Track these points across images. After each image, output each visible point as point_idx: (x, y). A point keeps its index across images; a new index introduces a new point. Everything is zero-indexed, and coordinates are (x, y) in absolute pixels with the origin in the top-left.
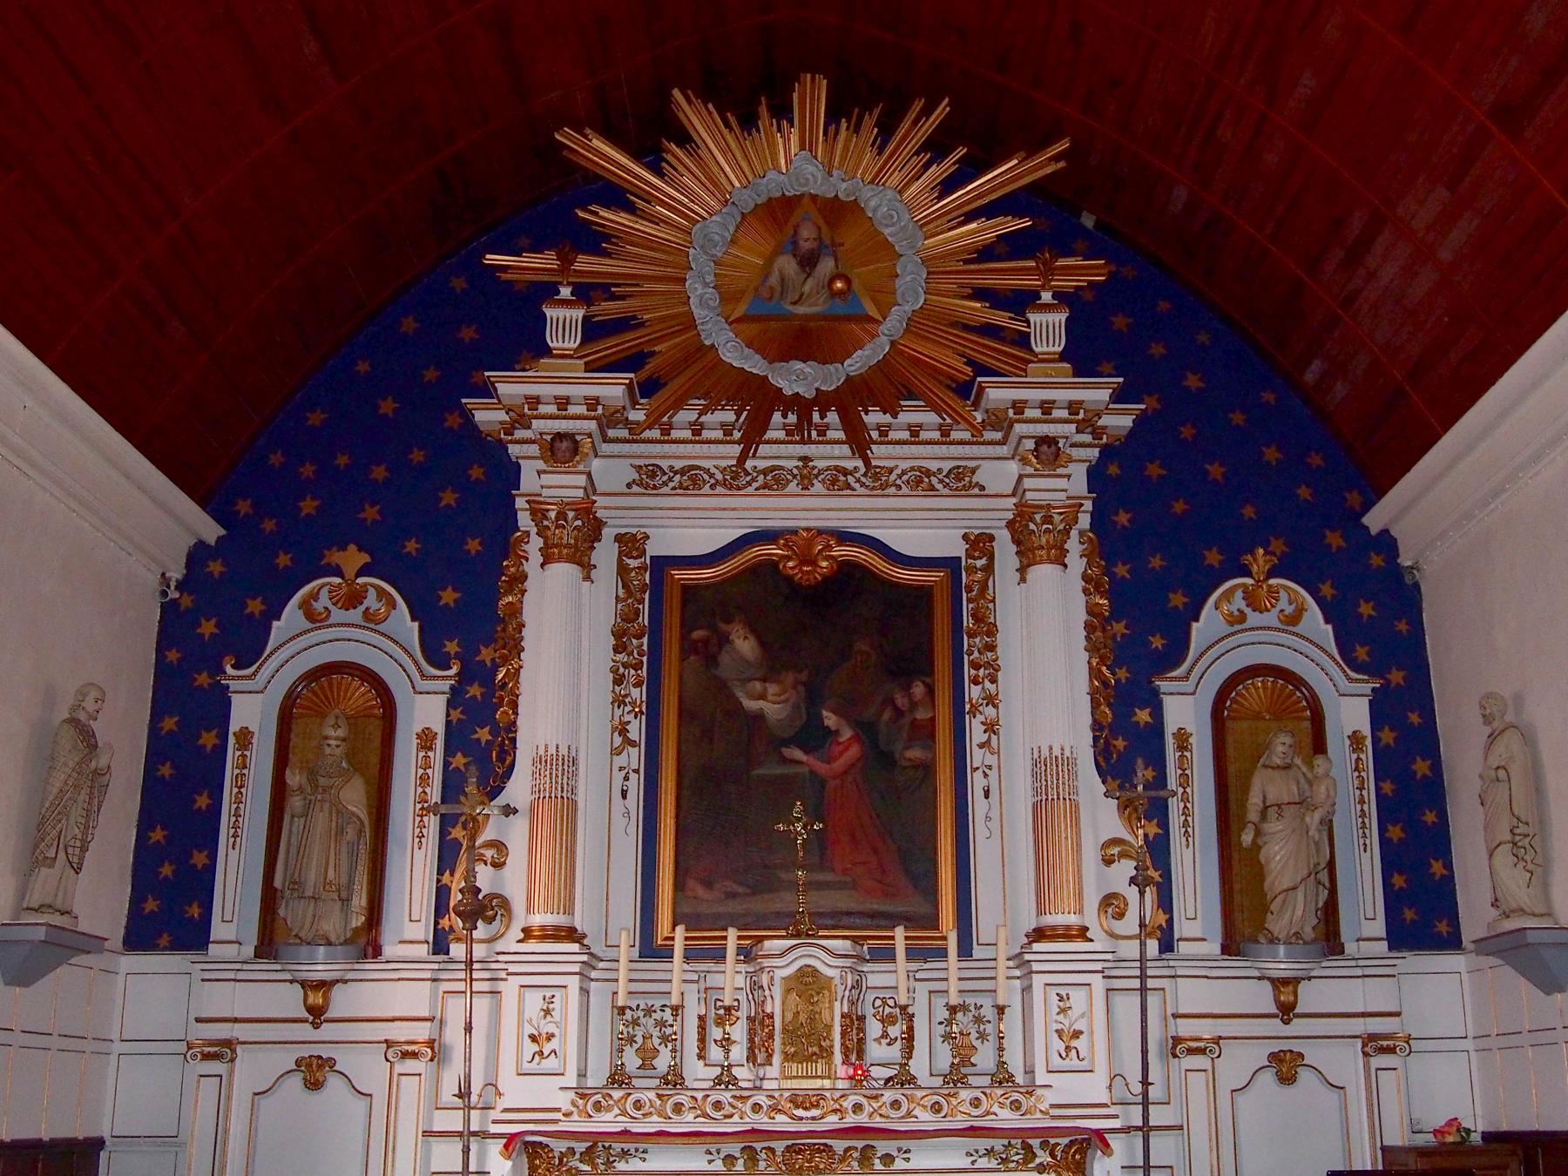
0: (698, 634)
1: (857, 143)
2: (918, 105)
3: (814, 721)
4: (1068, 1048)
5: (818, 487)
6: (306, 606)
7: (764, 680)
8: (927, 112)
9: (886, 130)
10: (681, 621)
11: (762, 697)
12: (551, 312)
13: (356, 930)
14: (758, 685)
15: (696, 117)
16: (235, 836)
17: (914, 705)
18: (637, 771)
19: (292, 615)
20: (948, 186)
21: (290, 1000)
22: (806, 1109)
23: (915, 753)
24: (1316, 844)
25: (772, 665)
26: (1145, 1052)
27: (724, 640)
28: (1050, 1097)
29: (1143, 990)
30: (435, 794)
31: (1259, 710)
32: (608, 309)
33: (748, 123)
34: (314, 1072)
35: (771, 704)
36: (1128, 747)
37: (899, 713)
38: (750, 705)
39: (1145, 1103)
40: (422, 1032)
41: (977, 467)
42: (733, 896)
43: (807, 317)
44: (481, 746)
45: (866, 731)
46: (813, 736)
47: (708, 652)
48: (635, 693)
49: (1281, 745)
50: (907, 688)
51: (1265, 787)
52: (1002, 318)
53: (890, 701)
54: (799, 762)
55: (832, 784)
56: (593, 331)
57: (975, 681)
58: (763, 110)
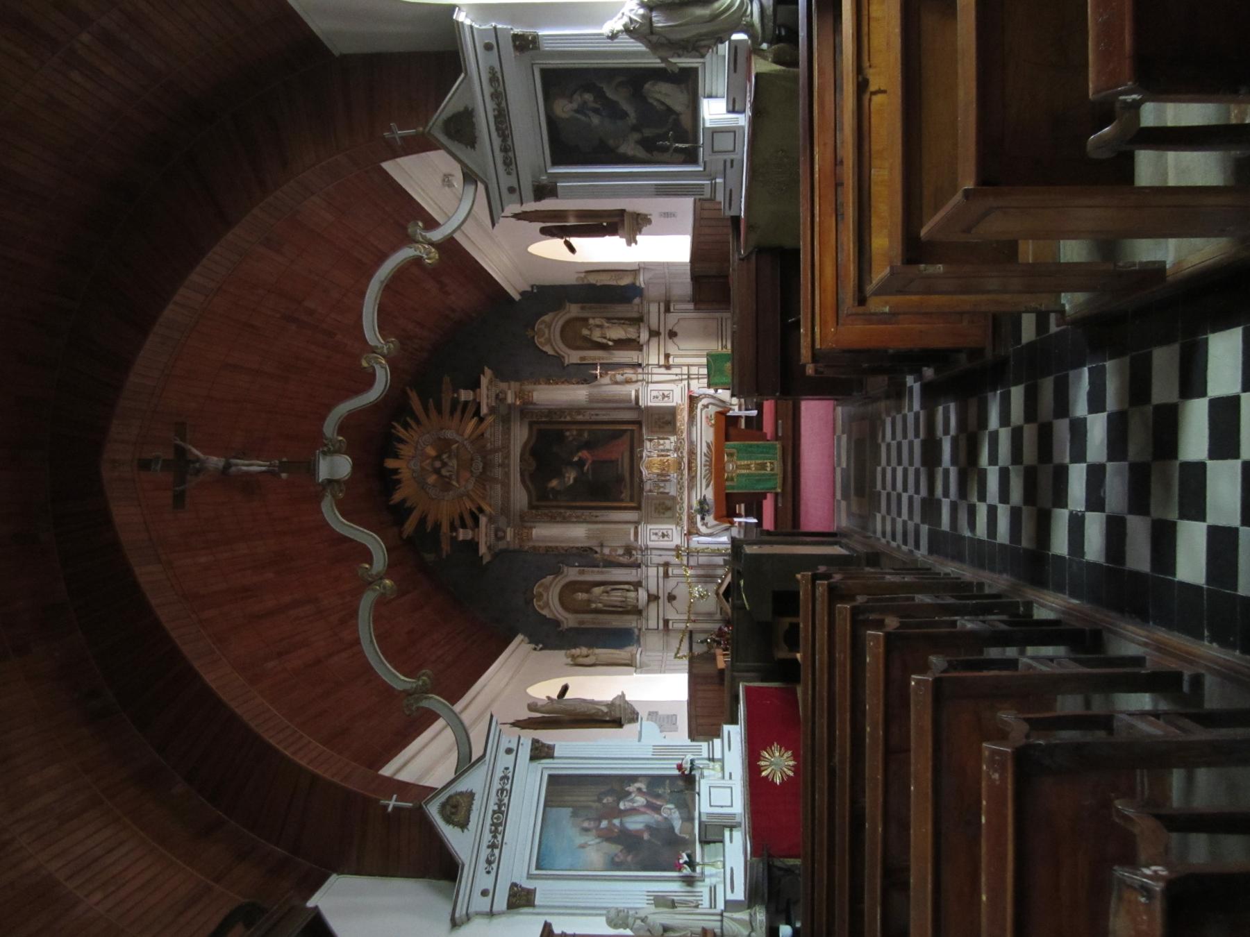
6: (542, 609)
9: (402, 441)
10: (546, 503)
12: (461, 538)
15: (397, 497)
21: (653, 606)
23: (586, 435)
25: (559, 474)
32: (457, 522)
34: (671, 598)
35: (571, 476)
36: (583, 375)
38: (572, 481)
44: (585, 556)
45: (579, 449)
46: (581, 463)
49: (585, 332)
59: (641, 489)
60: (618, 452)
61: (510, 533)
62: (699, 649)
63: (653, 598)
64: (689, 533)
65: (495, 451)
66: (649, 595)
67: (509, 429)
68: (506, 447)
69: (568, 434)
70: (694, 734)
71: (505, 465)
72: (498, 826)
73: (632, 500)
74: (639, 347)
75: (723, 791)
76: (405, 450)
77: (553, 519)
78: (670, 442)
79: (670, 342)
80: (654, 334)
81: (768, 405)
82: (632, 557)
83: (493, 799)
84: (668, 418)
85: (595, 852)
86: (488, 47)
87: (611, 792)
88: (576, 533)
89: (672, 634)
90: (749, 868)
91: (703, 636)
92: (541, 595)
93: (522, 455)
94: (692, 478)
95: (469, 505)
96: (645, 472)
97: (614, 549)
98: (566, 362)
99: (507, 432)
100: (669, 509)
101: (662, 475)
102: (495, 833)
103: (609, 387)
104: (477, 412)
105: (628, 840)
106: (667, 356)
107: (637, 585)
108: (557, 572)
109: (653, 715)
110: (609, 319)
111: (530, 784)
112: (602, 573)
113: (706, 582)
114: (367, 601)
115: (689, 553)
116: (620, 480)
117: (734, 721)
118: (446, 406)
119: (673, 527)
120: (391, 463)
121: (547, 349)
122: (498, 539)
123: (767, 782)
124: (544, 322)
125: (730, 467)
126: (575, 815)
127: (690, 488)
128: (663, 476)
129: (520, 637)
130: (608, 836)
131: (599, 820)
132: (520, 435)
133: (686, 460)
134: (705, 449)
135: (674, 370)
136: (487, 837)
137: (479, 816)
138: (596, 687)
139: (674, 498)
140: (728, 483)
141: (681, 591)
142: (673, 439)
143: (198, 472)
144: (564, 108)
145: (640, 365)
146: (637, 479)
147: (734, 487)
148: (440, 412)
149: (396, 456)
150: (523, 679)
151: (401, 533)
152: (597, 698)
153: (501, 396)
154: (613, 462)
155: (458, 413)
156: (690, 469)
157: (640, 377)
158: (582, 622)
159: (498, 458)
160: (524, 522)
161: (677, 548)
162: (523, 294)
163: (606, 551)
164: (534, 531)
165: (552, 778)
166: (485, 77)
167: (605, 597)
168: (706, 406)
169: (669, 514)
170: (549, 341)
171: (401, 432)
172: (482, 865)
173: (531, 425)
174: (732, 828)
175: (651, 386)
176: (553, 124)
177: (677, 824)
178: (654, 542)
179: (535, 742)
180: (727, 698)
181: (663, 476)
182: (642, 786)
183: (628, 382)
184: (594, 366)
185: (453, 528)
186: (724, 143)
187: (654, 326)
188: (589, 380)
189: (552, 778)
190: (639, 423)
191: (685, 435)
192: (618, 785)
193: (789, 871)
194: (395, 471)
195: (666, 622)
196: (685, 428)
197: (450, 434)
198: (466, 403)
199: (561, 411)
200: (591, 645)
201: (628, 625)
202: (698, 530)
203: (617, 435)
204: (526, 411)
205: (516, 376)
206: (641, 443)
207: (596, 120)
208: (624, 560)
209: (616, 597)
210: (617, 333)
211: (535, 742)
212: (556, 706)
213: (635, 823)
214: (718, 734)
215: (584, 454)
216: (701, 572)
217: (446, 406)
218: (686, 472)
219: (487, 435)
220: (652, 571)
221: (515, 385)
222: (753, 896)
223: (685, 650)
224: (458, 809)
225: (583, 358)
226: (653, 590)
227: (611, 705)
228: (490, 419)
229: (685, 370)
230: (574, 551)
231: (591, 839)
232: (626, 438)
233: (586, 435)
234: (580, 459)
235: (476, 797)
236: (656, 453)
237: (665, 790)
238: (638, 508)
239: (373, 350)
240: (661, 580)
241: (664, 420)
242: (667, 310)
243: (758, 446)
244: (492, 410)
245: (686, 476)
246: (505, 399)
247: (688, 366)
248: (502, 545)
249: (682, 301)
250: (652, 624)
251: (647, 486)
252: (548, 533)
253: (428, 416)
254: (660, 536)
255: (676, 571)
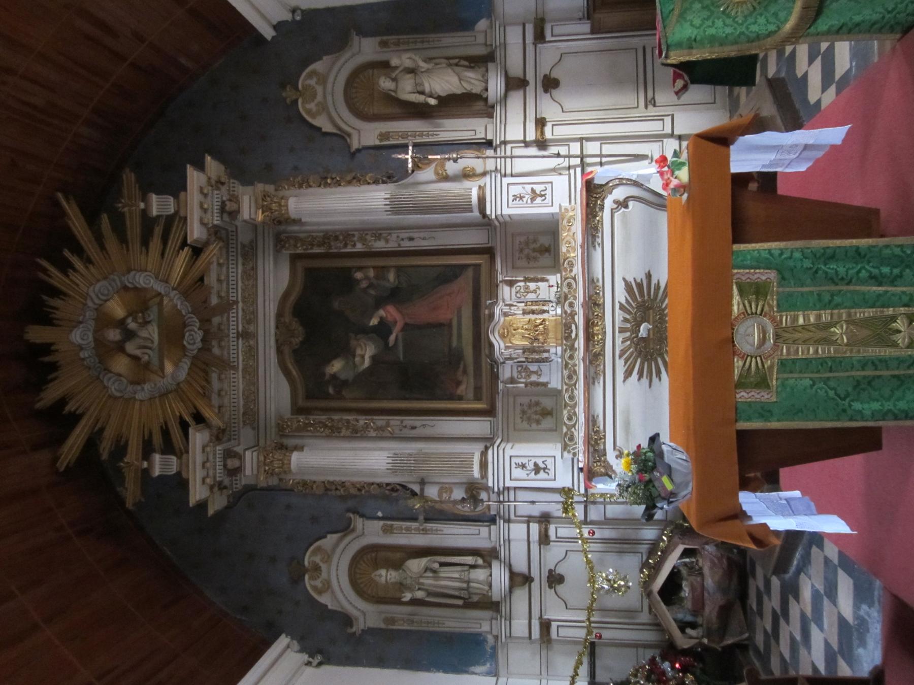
0: (331, 390)
1: (62, 308)
2: (41, 275)
3: (375, 329)
4: (542, 196)
5: (251, 328)
6: (320, 592)
7: (354, 356)
8: (45, 271)
9: (56, 292)
10: (321, 402)
11: (363, 357)
12: (157, 472)
13: (484, 561)
14: (357, 359)
15: (51, 394)
16: (438, 623)
17: (367, 278)
18: (402, 421)
20: (88, 261)
21: (520, 595)
22: (572, 331)
23: (391, 276)
24: (436, 64)
25: (347, 352)
26: (544, 157)
27: (334, 377)
28: (565, 204)
29: (512, 157)
30: (414, 525)
31: (365, 97)
32: (157, 439)
33: (54, 367)
34: (555, 579)
35: (366, 353)
36: (382, 166)
37: (371, 286)
38: (367, 363)
39: (569, 156)
40: (535, 527)
41: (241, 244)
42: (465, 372)
43: (160, 334)
45: (380, 303)
46: (383, 330)
47: (340, 384)
48: (362, 422)
49: (385, 84)
50: (358, 282)
52: (158, 231)
53: (365, 290)
54: (397, 336)
55: (408, 321)
56: (168, 448)
57: (354, 245)
58: (47, 359)
59: (495, 377)
61: (250, 460)
63: (519, 579)
66: (513, 575)
67: (254, 269)
68: (251, 298)
69: (359, 275)
73: (478, 398)
74: (488, 111)
77: (333, 432)
78: (547, 288)
80: (515, 84)
81: (834, 135)
82: (478, 504)
84: (545, 241)
88: (371, 459)
89: (556, 647)
92: (317, 568)
93: (279, 315)
94: (594, 358)
96: (496, 340)
97: (445, 488)
98: (355, 145)
99: (251, 274)
100: (546, 413)
101: (532, 350)
103: (427, 183)
106: (541, 123)
107: (488, 556)
110: (428, 60)
112: (425, 531)
113: (621, 552)
116: (455, 358)
118: (134, 230)
121: (322, 122)
124: (314, 73)
127: (590, 382)
128: (535, 353)
129: (283, 640)
132: (275, 280)
133: (580, 320)
134: (621, 296)
139: (557, 393)
140: (743, 396)
141: (574, 568)
142: (554, 279)
145: (489, 144)
146: (485, 362)
147: (765, 408)
148: (123, 240)
151: (55, 459)
153: (230, 206)
154: (442, 327)
155: (155, 244)
156: (589, 337)
157: (490, 164)
158: (390, 620)
160: (283, 442)
162: (277, 27)
167: (428, 581)
168: (623, 204)
169: (547, 423)
170: (323, 108)
171: (56, 277)
173: (294, 258)
178: (521, 477)
181: (535, 353)
183: (467, 175)
187: (515, 70)
188: (394, 174)
190: (489, 252)
191: (577, 270)
195: (546, 626)
196: (576, 255)
197: (141, 280)
201: (474, 628)
202: (608, 467)
203: (450, 275)
204: (281, 231)
205: (269, 174)
206: (493, 293)
208: (466, 509)
210: (445, 82)
215: (389, 312)
216: (608, 533)
217: (134, 230)
218: (580, 343)
219: (211, 279)
220: (518, 531)
225: (384, 136)
226: (520, 566)
228: (213, 251)
230: (374, 490)
232: (465, 282)
233: (391, 276)
234: (382, 321)
236: (521, 310)
238: (490, 412)
240: (535, 548)
241: (537, 245)
242: (540, 37)
243: (859, 255)
245: (581, 352)
246: (238, 212)
247: (581, 140)
249: (567, 19)
250: (519, 626)
251: (506, 372)
253: (102, 247)
254: (530, 466)
255: (564, 532)
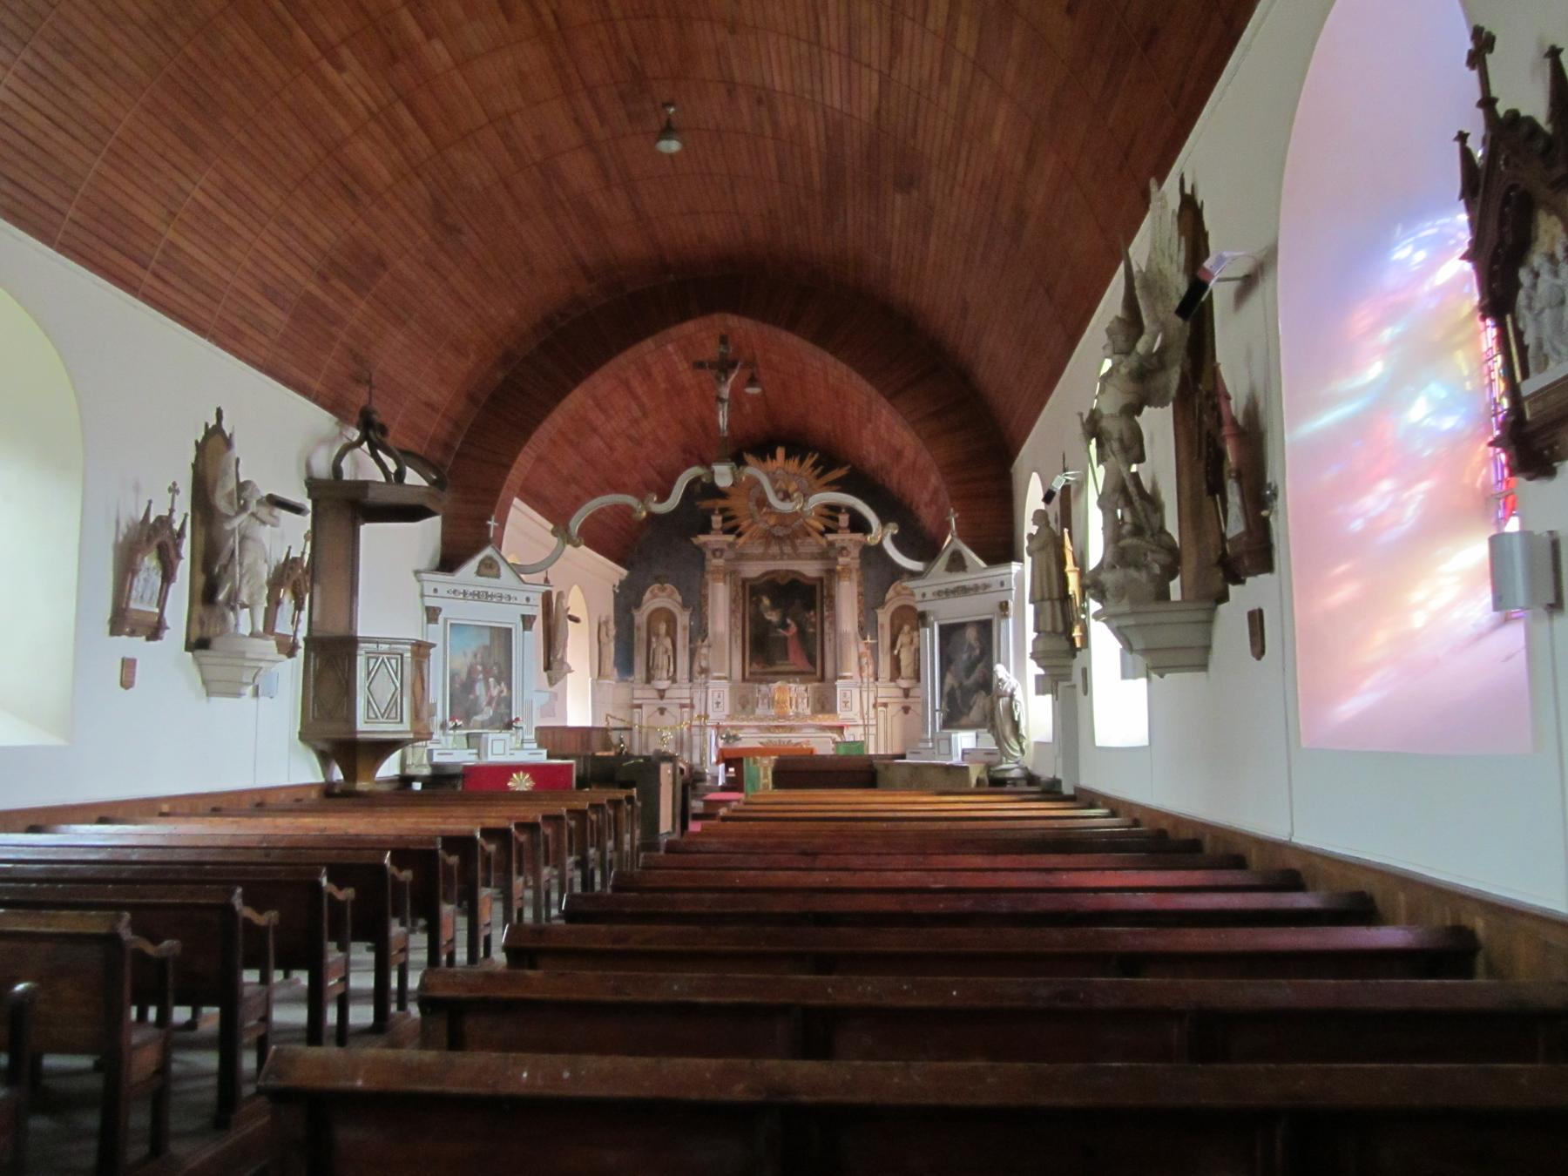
9: (801, 461)
10: (750, 592)
19: (648, 595)
20: (818, 477)
21: (655, 694)
25: (774, 606)
32: (728, 514)
34: (662, 711)
35: (773, 617)
36: (867, 626)
44: (699, 631)
45: (799, 625)
47: (758, 603)
49: (906, 628)
51: (902, 639)
59: (760, 682)
60: (796, 660)
61: (719, 562)
62: (614, 737)
63: (662, 694)
64: (718, 727)
65: (794, 547)
68: (797, 556)
70: (541, 731)
71: (782, 556)
72: (478, 596)
74: (893, 679)
75: (501, 749)
76: (793, 465)
79: (898, 707)
82: (699, 673)
83: (496, 591)
85: (461, 663)
86: (1002, 584)
87: (500, 672)
90: (455, 764)
91: (627, 741)
93: (793, 572)
94: (769, 729)
95: (745, 524)
96: (775, 686)
97: (706, 657)
99: (814, 557)
100: (744, 707)
102: (473, 594)
104: (829, 530)
105: (468, 686)
106: (885, 705)
107: (674, 680)
108: (685, 605)
109: (555, 696)
111: (508, 616)
114: (630, 500)
115: (702, 728)
116: (769, 661)
117: (549, 757)
119: (727, 712)
120: (780, 452)
122: (714, 552)
123: (509, 777)
125: (766, 762)
126: (485, 648)
127: (758, 727)
129: (625, 572)
130: (471, 671)
131: (482, 664)
132: (811, 569)
134: (794, 741)
135: (872, 712)
136: (471, 589)
137: (485, 584)
138: (579, 648)
139: (753, 712)
141: (668, 719)
142: (808, 712)
143: (718, 378)
144: (971, 634)
146: (770, 678)
147: (748, 765)
149: (788, 456)
150: (586, 582)
152: (569, 650)
154: (786, 655)
159: (787, 549)
160: (730, 574)
161: (707, 717)
163: (704, 651)
164: (721, 584)
165: (510, 630)
166: (986, 581)
167: (661, 650)
169: (739, 707)
171: (809, 462)
172: (453, 588)
173: (821, 580)
174: (478, 754)
175: (856, 692)
176: (961, 626)
177: (478, 718)
179: (534, 617)
180: (566, 752)
182: (505, 693)
183: (861, 669)
184: (875, 636)
185: (722, 511)
186: (943, 747)
189: (510, 630)
190: (822, 679)
192: (505, 676)
193: (455, 787)
194: (773, 457)
195: (640, 706)
198: (837, 520)
199: (832, 607)
200: (617, 637)
201: (636, 670)
203: (811, 660)
207: (965, 656)
208: (696, 668)
209: (662, 660)
211: (534, 617)
212: (562, 616)
213: (480, 689)
214: (540, 746)
215: (793, 628)
219: (809, 540)
221: (856, 564)
222: (436, 767)
223: (613, 723)
224: (489, 568)
226: (668, 694)
227: (563, 661)
228: (823, 542)
229: (872, 722)
231: (469, 659)
232: (808, 668)
235: (493, 581)
236: (795, 695)
237: (503, 709)
239: (806, 501)
241: (825, 704)
244: (831, 544)
248: (709, 555)
250: (638, 693)
251: (764, 688)
252: (720, 597)
254: (718, 698)
